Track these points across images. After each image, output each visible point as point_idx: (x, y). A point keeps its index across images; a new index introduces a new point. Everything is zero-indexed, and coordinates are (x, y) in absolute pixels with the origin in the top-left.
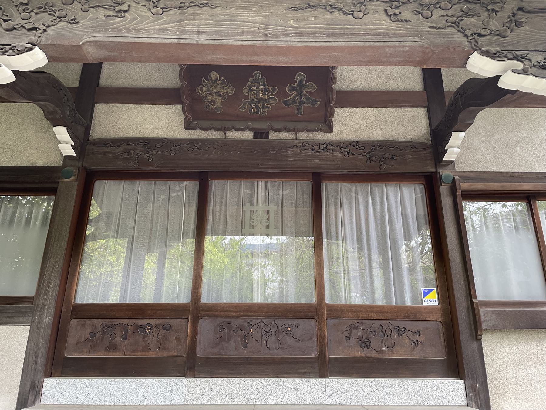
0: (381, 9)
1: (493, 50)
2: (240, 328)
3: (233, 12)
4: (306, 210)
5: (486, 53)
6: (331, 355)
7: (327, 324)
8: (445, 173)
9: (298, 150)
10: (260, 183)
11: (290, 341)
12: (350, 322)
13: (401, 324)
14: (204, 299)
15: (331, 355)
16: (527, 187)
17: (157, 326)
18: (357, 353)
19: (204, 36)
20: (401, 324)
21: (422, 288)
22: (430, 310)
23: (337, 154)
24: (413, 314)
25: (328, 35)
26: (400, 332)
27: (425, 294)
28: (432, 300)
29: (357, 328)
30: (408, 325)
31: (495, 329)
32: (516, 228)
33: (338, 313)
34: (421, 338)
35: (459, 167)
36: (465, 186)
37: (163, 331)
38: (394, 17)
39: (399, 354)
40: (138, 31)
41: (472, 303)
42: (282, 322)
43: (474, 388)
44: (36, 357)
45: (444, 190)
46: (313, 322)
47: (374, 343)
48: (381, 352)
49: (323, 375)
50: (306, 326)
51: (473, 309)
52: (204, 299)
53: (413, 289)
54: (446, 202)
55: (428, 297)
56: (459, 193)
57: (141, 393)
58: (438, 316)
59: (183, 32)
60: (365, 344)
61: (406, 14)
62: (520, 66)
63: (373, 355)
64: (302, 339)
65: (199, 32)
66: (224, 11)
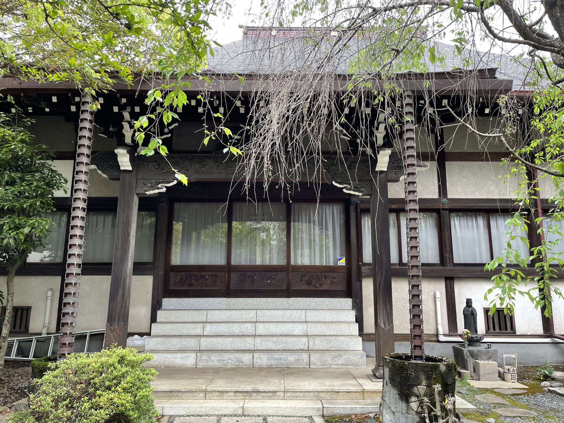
12: (302, 273)
13: (327, 274)
17: (211, 275)
18: (305, 287)
20: (327, 274)
27: (340, 260)
28: (342, 262)
30: (330, 274)
34: (335, 281)
39: (325, 287)
40: (211, 173)
45: (352, 208)
46: (285, 273)
47: (314, 282)
48: (316, 287)
55: (341, 261)
56: (359, 210)
60: (309, 283)
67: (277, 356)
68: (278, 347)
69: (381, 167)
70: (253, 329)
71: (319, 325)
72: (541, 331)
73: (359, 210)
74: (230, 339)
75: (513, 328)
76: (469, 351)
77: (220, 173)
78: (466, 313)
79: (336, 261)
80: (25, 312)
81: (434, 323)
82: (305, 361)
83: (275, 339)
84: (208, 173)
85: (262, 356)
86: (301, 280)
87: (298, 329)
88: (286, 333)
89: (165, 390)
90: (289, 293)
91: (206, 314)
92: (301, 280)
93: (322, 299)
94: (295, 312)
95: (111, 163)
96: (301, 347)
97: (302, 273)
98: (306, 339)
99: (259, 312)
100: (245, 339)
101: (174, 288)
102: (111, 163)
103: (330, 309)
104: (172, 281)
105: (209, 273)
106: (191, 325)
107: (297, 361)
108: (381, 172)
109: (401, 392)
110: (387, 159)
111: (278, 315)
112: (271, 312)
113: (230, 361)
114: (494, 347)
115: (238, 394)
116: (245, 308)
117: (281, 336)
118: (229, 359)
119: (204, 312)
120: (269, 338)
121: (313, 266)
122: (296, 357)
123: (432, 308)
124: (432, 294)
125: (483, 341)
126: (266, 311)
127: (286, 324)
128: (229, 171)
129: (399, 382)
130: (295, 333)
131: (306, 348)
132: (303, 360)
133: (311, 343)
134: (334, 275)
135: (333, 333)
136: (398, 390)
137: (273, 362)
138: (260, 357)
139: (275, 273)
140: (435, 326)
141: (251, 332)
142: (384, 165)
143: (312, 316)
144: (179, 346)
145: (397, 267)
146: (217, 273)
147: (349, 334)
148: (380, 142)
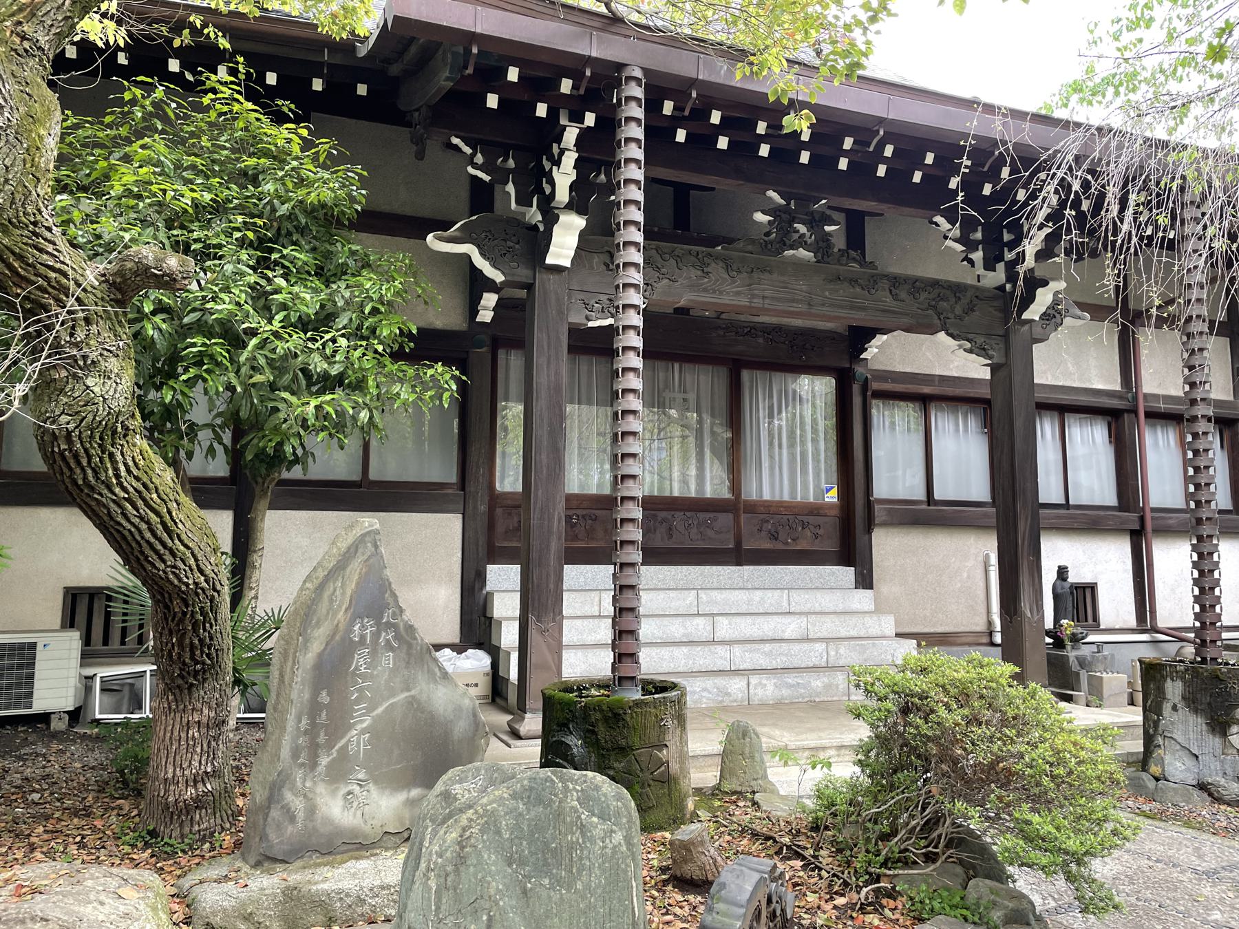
0: (887, 287)
1: (955, 333)
2: (664, 520)
3: (785, 279)
4: (722, 403)
5: (948, 334)
6: (746, 546)
7: (743, 518)
8: (859, 370)
9: (721, 333)
10: (702, 377)
11: (710, 533)
12: (762, 516)
13: (805, 519)
14: (373, 475)
15: (746, 546)
16: (927, 390)
17: (583, 517)
18: (767, 545)
19: (767, 301)
20: (805, 519)
21: (824, 486)
22: (831, 505)
23: (761, 340)
24: (815, 510)
25: (852, 308)
26: (804, 525)
27: (828, 491)
28: (832, 496)
29: (768, 521)
30: (811, 519)
31: (884, 524)
32: (909, 430)
33: (753, 508)
34: (821, 532)
35: (874, 366)
36: (875, 386)
37: (589, 522)
38: (895, 297)
39: (802, 545)
40: (721, 293)
41: (869, 501)
42: (702, 516)
43: (862, 574)
44: (477, 545)
45: (856, 388)
46: (731, 516)
47: (782, 536)
48: (787, 544)
49: (739, 564)
50: (725, 519)
51: (869, 505)
52: (373, 475)
53: (817, 486)
54: (857, 401)
55: (829, 494)
56: (869, 393)
57: (582, 579)
58: (836, 512)
59: (753, 296)
60: (774, 537)
61: (903, 295)
62: (968, 345)
63: (781, 547)
64: (721, 530)
65: (764, 297)
66: (782, 278)
67: (791, 679)
68: (774, 664)
69: (558, 256)
70: (709, 628)
71: (827, 619)
72: (1132, 622)
73: (869, 393)
74: (685, 649)
75: (1096, 618)
76: (1077, 658)
77: (738, 294)
78: (1059, 591)
79: (820, 493)
80: (98, 606)
81: (984, 611)
82: (841, 687)
83: (767, 647)
84: (714, 292)
85: (764, 682)
86: (760, 530)
87: (791, 627)
88: (770, 635)
89: (711, 752)
90: (738, 556)
91: (597, 599)
92: (760, 530)
93: (588, 567)
94: (769, 593)
95: (509, 244)
96: (815, 661)
97: (762, 516)
98: (824, 645)
99: (702, 594)
100: (712, 648)
101: (506, 544)
102: (509, 244)
103: (817, 588)
104: (500, 528)
105: (579, 512)
106: (586, 622)
107: (828, 687)
108: (558, 269)
109: (1212, 718)
110: (573, 241)
111: (739, 599)
112: (726, 594)
113: (705, 694)
114: (1107, 651)
115: (843, 751)
116: (660, 585)
117: (763, 641)
118: (704, 690)
119: (593, 594)
120: (757, 646)
121: (780, 504)
122: (826, 680)
123: (982, 584)
124: (981, 559)
125: (1088, 640)
126: (715, 592)
127: (769, 618)
128: (756, 292)
129: (1209, 704)
130: (786, 636)
131: (824, 664)
132: (837, 686)
133: (832, 653)
134: (820, 520)
135: (853, 633)
136: (1207, 718)
137: (785, 692)
138: (760, 683)
139: (712, 515)
140: (985, 617)
141: (705, 635)
142: (564, 252)
143: (800, 600)
144: (583, 667)
145: (924, 507)
146: (598, 512)
147: (879, 634)
148: (562, 196)
